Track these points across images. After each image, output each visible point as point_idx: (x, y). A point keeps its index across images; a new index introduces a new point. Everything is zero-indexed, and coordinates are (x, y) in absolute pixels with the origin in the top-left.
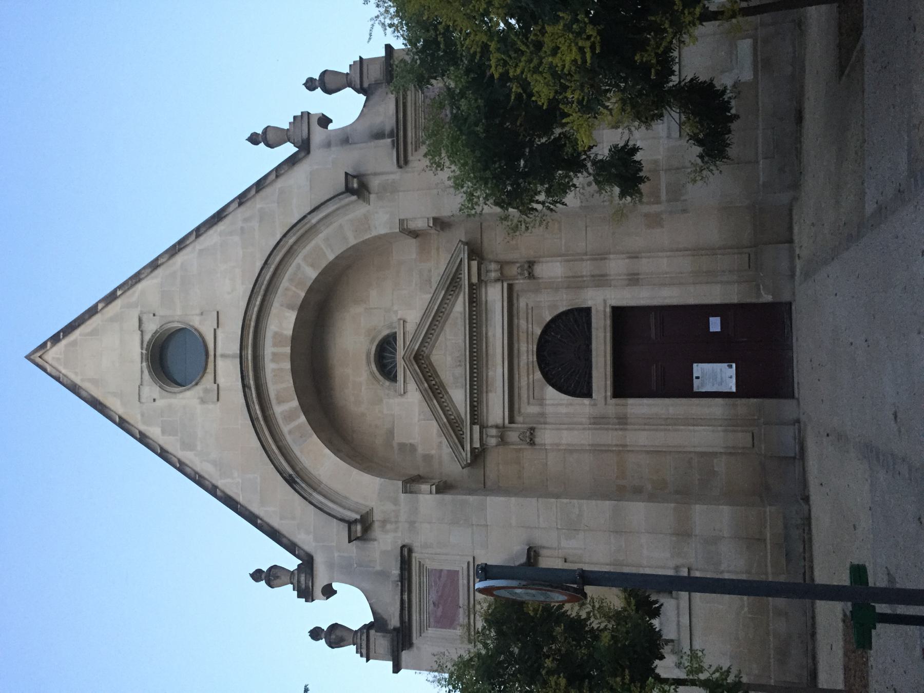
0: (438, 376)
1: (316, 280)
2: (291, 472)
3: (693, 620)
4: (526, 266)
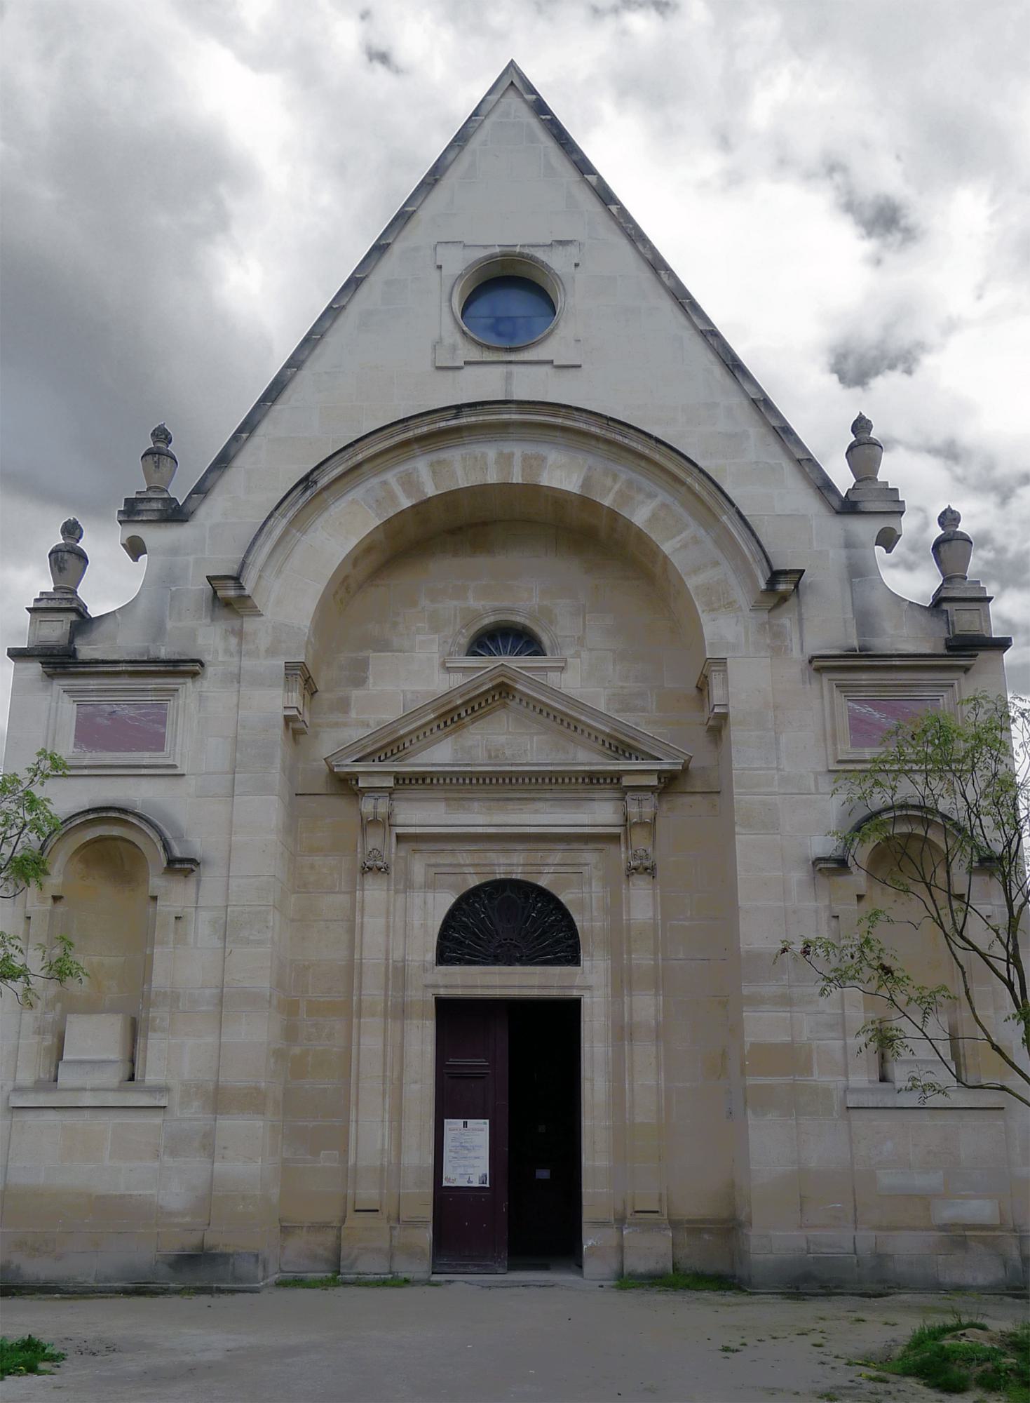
0: (473, 721)
1: (629, 525)
2: (323, 482)
4: (647, 863)
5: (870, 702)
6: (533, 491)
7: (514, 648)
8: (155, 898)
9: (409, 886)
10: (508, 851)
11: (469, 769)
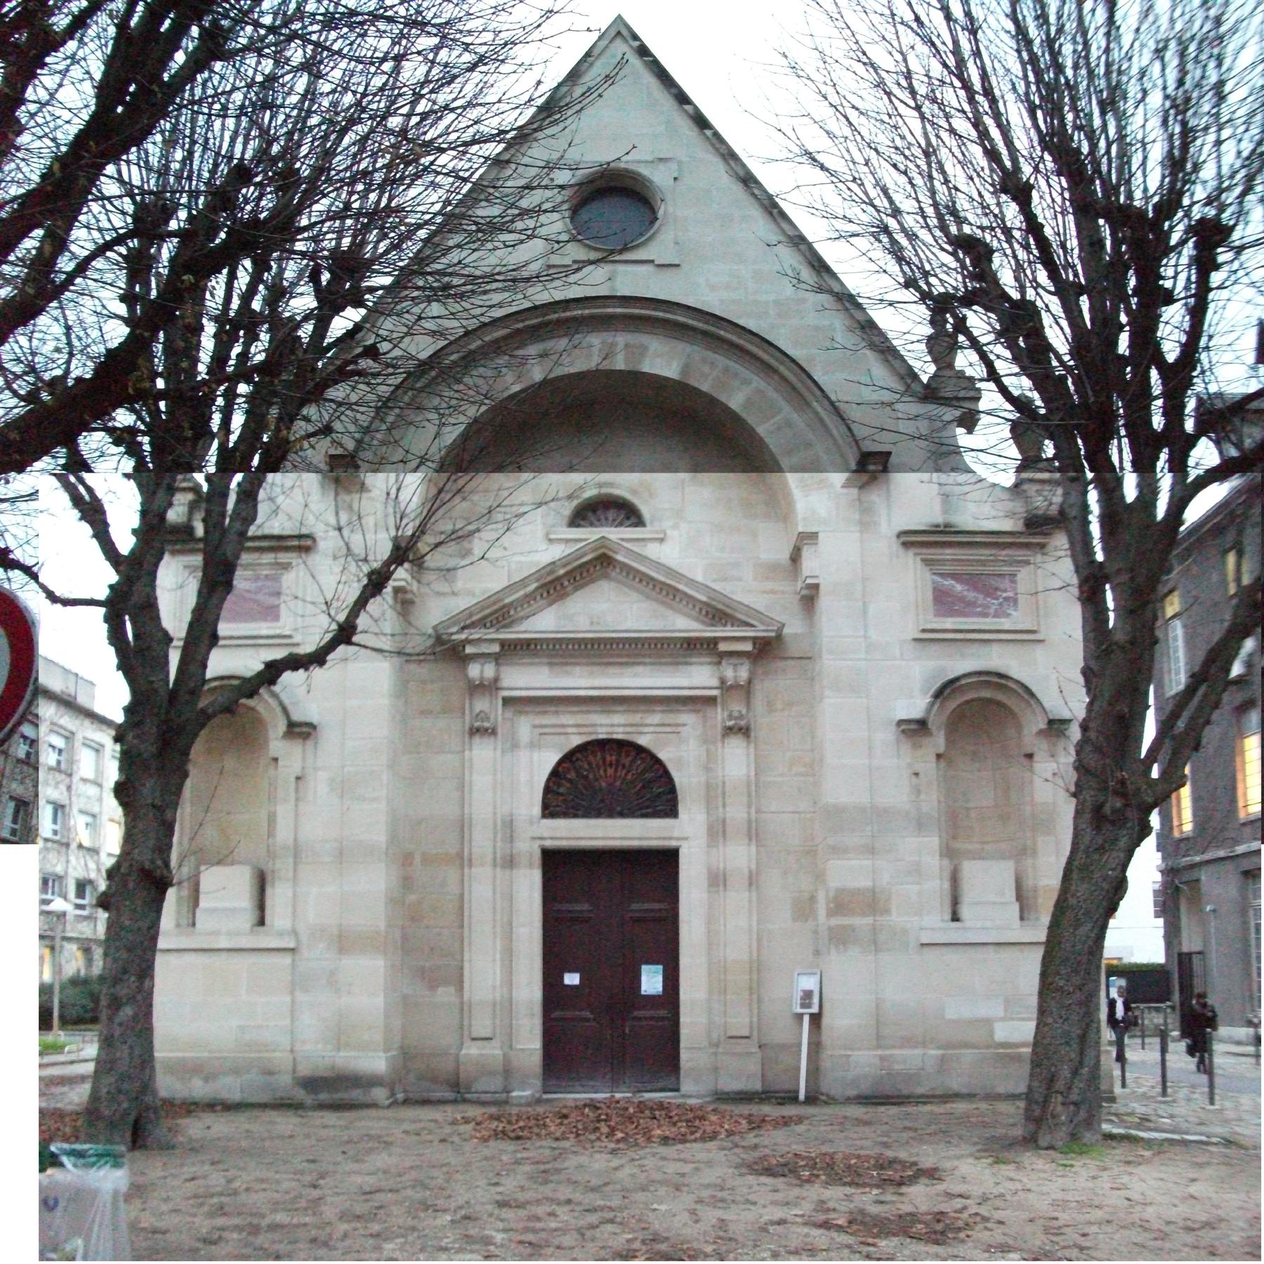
0: (576, 589)
1: (726, 409)
3: (224, 955)
4: (742, 723)
5: (954, 576)
6: (635, 377)
7: (614, 520)
8: (276, 760)
9: (515, 746)
10: (609, 712)
11: (572, 635)
